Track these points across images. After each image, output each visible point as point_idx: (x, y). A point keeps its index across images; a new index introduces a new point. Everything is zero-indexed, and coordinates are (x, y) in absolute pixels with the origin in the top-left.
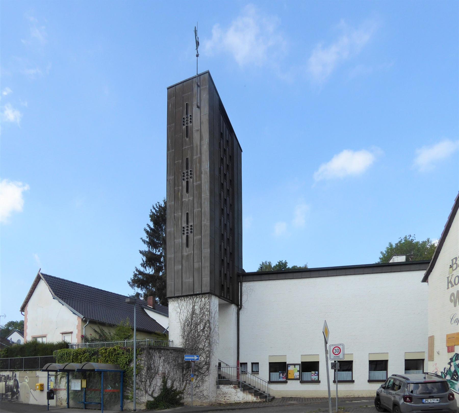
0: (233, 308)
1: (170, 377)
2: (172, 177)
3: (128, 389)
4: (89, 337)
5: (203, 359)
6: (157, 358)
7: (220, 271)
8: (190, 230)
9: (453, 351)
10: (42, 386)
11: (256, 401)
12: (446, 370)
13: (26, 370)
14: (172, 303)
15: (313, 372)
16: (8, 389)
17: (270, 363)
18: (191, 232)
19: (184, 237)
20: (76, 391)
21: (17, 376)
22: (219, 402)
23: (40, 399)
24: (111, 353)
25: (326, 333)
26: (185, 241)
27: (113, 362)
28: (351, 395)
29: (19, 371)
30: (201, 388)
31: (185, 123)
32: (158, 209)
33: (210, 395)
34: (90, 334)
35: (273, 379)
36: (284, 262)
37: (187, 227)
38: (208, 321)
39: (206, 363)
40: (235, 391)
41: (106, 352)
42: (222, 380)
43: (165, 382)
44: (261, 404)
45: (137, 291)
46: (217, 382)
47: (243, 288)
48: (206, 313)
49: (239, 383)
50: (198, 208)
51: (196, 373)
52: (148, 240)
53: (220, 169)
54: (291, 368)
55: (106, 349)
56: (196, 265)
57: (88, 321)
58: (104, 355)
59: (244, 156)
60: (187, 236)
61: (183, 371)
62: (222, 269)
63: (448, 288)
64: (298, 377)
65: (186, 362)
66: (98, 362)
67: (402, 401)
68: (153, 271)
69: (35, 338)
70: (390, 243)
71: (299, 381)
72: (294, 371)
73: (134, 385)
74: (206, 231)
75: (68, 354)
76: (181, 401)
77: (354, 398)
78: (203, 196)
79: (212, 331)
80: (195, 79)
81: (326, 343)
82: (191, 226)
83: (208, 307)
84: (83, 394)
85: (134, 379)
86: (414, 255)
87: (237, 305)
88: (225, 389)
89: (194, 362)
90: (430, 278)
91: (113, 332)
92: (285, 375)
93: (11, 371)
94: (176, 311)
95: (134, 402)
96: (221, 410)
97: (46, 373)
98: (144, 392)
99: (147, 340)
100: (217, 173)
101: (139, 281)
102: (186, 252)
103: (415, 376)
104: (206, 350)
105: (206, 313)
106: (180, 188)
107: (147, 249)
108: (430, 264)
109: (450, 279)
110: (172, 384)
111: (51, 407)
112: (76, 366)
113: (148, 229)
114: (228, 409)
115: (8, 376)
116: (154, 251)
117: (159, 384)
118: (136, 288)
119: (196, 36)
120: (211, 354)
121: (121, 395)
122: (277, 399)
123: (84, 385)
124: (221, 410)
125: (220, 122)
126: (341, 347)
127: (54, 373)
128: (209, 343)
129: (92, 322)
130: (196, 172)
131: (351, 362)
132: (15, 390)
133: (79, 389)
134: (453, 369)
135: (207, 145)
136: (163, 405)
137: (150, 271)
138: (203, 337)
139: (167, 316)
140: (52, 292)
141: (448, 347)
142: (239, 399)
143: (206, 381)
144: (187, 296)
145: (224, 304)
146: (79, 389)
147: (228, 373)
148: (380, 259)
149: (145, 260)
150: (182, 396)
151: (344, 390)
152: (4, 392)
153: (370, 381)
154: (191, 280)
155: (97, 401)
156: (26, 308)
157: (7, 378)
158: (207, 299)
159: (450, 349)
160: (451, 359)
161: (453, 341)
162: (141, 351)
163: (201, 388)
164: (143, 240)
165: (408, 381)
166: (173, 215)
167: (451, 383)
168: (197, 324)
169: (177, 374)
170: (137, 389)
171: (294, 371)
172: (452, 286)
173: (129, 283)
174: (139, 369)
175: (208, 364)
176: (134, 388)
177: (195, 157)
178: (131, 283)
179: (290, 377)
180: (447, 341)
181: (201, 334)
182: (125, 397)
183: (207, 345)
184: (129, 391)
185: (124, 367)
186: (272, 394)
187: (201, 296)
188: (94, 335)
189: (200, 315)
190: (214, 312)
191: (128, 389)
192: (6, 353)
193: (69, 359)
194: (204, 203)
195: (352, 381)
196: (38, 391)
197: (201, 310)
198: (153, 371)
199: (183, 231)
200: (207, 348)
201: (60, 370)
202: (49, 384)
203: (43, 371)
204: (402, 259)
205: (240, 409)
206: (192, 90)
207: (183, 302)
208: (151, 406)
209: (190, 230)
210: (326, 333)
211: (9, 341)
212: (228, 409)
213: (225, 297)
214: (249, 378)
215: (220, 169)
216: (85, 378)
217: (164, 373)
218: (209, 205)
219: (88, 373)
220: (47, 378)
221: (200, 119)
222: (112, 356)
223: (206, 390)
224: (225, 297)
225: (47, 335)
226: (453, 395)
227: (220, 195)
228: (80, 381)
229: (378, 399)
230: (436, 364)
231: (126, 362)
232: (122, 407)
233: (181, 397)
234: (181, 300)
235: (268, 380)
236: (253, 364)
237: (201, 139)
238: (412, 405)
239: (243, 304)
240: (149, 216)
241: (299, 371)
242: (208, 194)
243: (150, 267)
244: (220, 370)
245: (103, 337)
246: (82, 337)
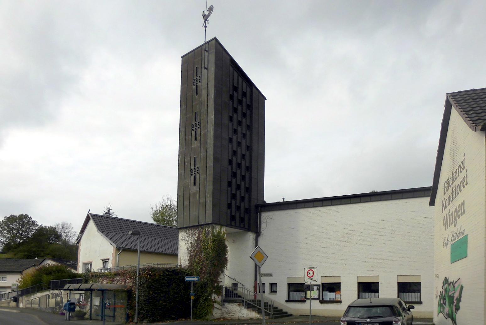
0: (251, 236)
19: (192, 178)
37: (195, 169)
40: (239, 309)
56: (202, 200)
57: (121, 250)
60: (194, 176)
71: (318, 301)
82: (198, 168)
106: (190, 137)
115: (57, 293)
126: (314, 270)
127: (83, 292)
131: (419, 284)
152: (55, 306)
157: (57, 296)
194: (209, 147)
214: (268, 296)
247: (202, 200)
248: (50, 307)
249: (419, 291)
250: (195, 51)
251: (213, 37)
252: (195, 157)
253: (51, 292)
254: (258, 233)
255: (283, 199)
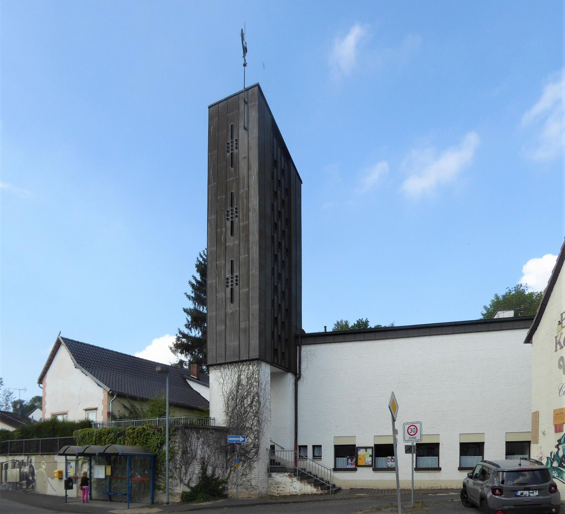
0: (290, 378)
1: (211, 462)
2: (214, 217)
3: (160, 478)
4: (116, 414)
5: (250, 441)
6: (194, 440)
7: (273, 333)
8: (235, 281)
9: (561, 430)
10: (60, 473)
11: (317, 493)
12: (553, 454)
13: (44, 454)
14: (213, 372)
15: (390, 457)
16: (23, 476)
17: (336, 446)
18: (236, 284)
20: (99, 480)
21: (33, 461)
22: (270, 494)
23: (54, 488)
24: (140, 434)
25: (393, 407)
26: (229, 295)
27: (143, 444)
28: (437, 486)
29: (34, 455)
30: (249, 476)
31: (230, 149)
32: (205, 257)
33: (259, 484)
34: (119, 410)
35: (339, 466)
36: (364, 320)
37: (232, 277)
38: (257, 393)
39: (254, 445)
40: (290, 481)
41: (134, 433)
42: (275, 466)
43: (204, 469)
44: (322, 497)
45: (180, 358)
46: (268, 469)
47: (302, 352)
48: (255, 384)
49: (295, 470)
50: (244, 254)
51: (243, 458)
52: (193, 295)
53: (273, 205)
54: (361, 452)
55: (134, 429)
56: (243, 325)
58: (131, 436)
59: (304, 188)
60: (232, 289)
61: (227, 456)
62: (276, 329)
63: (556, 350)
64: (370, 463)
65: (230, 444)
66: (124, 444)
67: (489, 494)
68: (200, 334)
69: (55, 416)
70: (496, 295)
71: (371, 469)
72: (365, 456)
73: (167, 473)
74: (255, 283)
75: (91, 435)
76: (225, 493)
77: (441, 489)
78: (251, 239)
79: (262, 405)
80: (241, 94)
81: (394, 420)
82: (236, 276)
83: (257, 376)
84: (108, 483)
85: (167, 466)
86: (525, 309)
87: (295, 374)
88: (281, 478)
89: (240, 444)
90: (534, 338)
91: (146, 408)
92: (354, 461)
93: (27, 455)
94: (218, 381)
95: (167, 493)
96: (271, 504)
97: (64, 457)
98: (178, 481)
99: (181, 416)
100: (269, 210)
101: (182, 346)
102: (231, 309)
103: (515, 463)
104: (254, 429)
105: (255, 384)
106: (224, 229)
107: (192, 307)
108: (534, 320)
109: (558, 339)
110: (214, 471)
111: (71, 498)
112: (96, 449)
113: (194, 282)
114: (280, 503)
116: (201, 309)
117: (197, 472)
118: (179, 354)
119: (243, 39)
120: (261, 435)
121: (151, 485)
122: (344, 490)
123: (109, 473)
124: (271, 504)
125: (273, 147)
127: (74, 458)
128: (258, 421)
129: (121, 396)
130: (243, 209)
131: (437, 445)
132: (31, 478)
133: (103, 476)
134: (561, 454)
135: (256, 176)
136: (202, 497)
137: (196, 333)
138: (250, 414)
139: (209, 387)
140: (74, 360)
141: (556, 426)
142: (295, 490)
143: (254, 467)
144: (231, 363)
145: (278, 373)
146: (103, 476)
147: (282, 457)
148: (483, 314)
149: (190, 320)
150: (226, 486)
151: (425, 480)
152: (18, 480)
153: (461, 469)
154: (236, 343)
155: (124, 491)
156: (44, 379)
157: (22, 464)
158: (255, 367)
159: (558, 429)
160: (559, 441)
161: (561, 418)
162: (175, 430)
163: (249, 476)
164: (187, 296)
165: (499, 469)
166: (215, 264)
167: (559, 471)
168: (243, 398)
169: (220, 460)
170: (172, 477)
171: (365, 456)
172: (562, 348)
173: (171, 349)
174: (172, 453)
175: (257, 447)
176: (167, 475)
177: (241, 191)
178: (174, 349)
179: (360, 463)
180: (555, 418)
181: (248, 410)
182: (156, 487)
183: (255, 424)
184: (161, 480)
185: (155, 450)
186: (338, 485)
187: (248, 363)
188: (123, 412)
189: (247, 386)
190: (264, 383)
191: (160, 478)
192: (21, 433)
193: (92, 441)
194: (252, 247)
195: (439, 469)
196: (57, 479)
197: (248, 381)
198: (189, 455)
199: (227, 282)
200: (256, 428)
201: (80, 454)
202: (69, 471)
203: (60, 455)
204: (510, 314)
205: (295, 502)
206: (239, 109)
207: (226, 371)
208: (187, 498)
209: (235, 282)
210: (393, 407)
211: (30, 419)
212: (280, 503)
213: (279, 363)
214: (309, 464)
215: (273, 205)
216: (109, 464)
217: (203, 458)
218: (258, 250)
219: (113, 458)
220: (64, 464)
221: (248, 143)
222: (141, 437)
223: (255, 478)
224: (279, 363)
225: (68, 411)
226: (555, 486)
227: (273, 237)
228: (104, 467)
229: (464, 491)
230: (541, 447)
231: (158, 445)
232: (153, 499)
233: (224, 488)
234: (224, 368)
235: (333, 467)
236: (314, 447)
237: (249, 168)
238: (503, 498)
239: (302, 373)
240: (195, 266)
241: (371, 456)
242: (257, 236)
243: (197, 329)
244: (274, 454)
245: (134, 414)
246: (109, 414)
247: (243, 325)
248: (10, 483)
249: (437, 455)
250: (229, 100)
251: (254, 83)
252: (232, 261)
253: (11, 458)
254: (298, 377)
255: (325, 327)
